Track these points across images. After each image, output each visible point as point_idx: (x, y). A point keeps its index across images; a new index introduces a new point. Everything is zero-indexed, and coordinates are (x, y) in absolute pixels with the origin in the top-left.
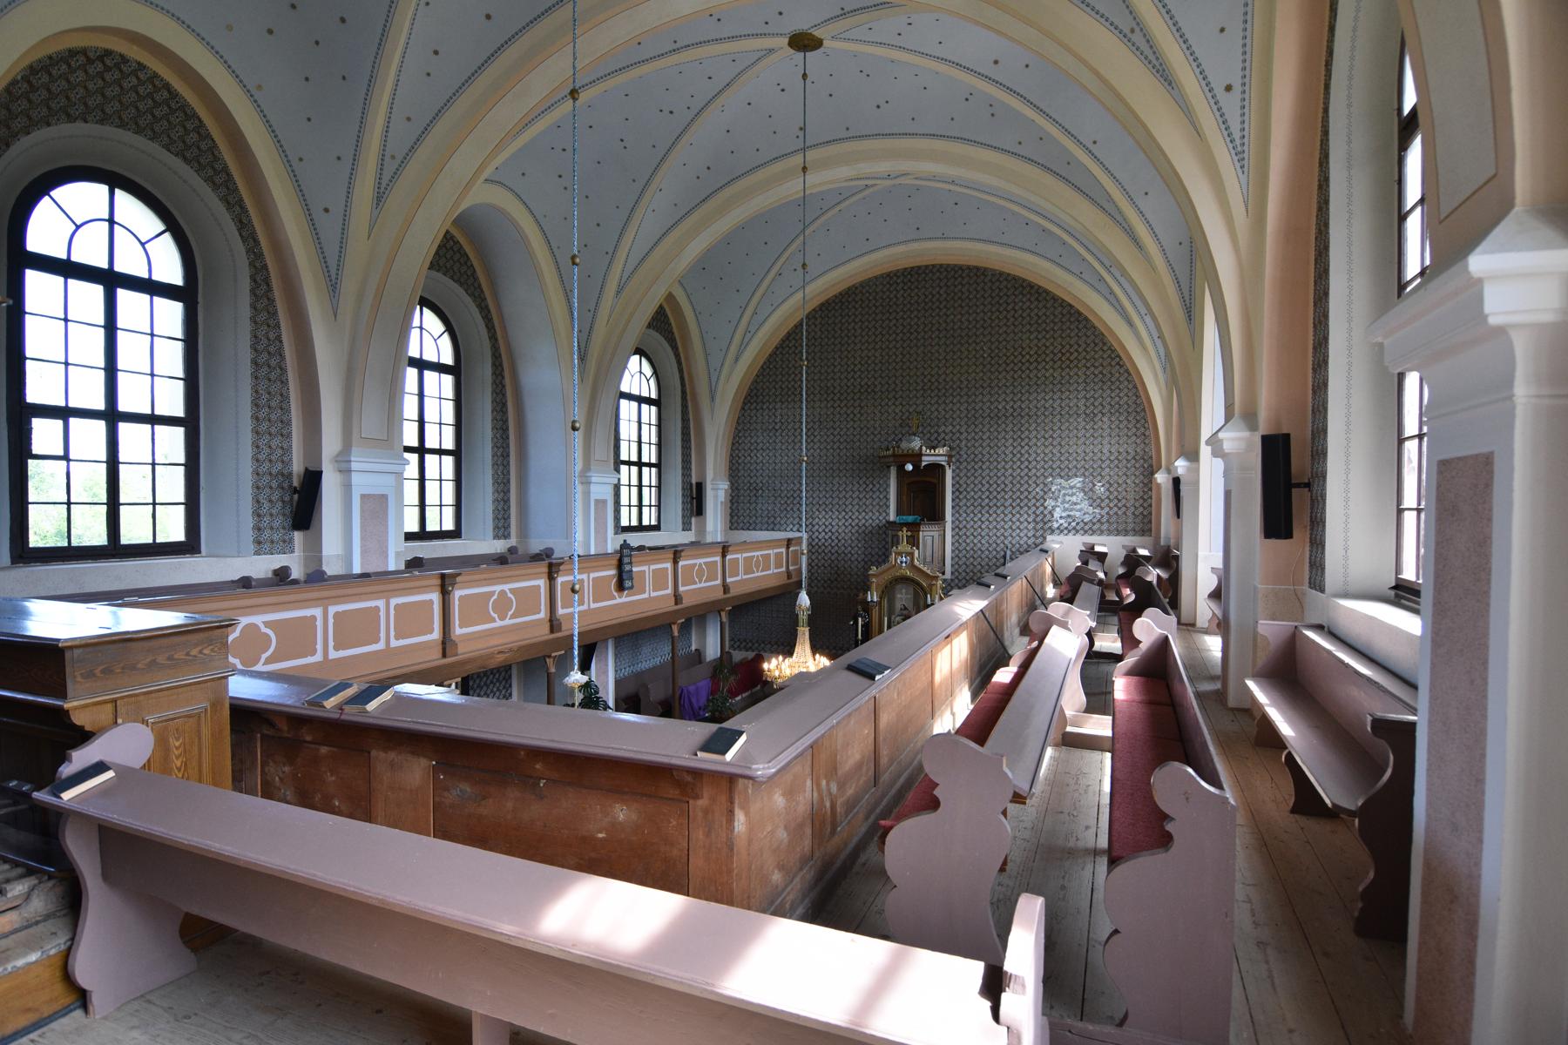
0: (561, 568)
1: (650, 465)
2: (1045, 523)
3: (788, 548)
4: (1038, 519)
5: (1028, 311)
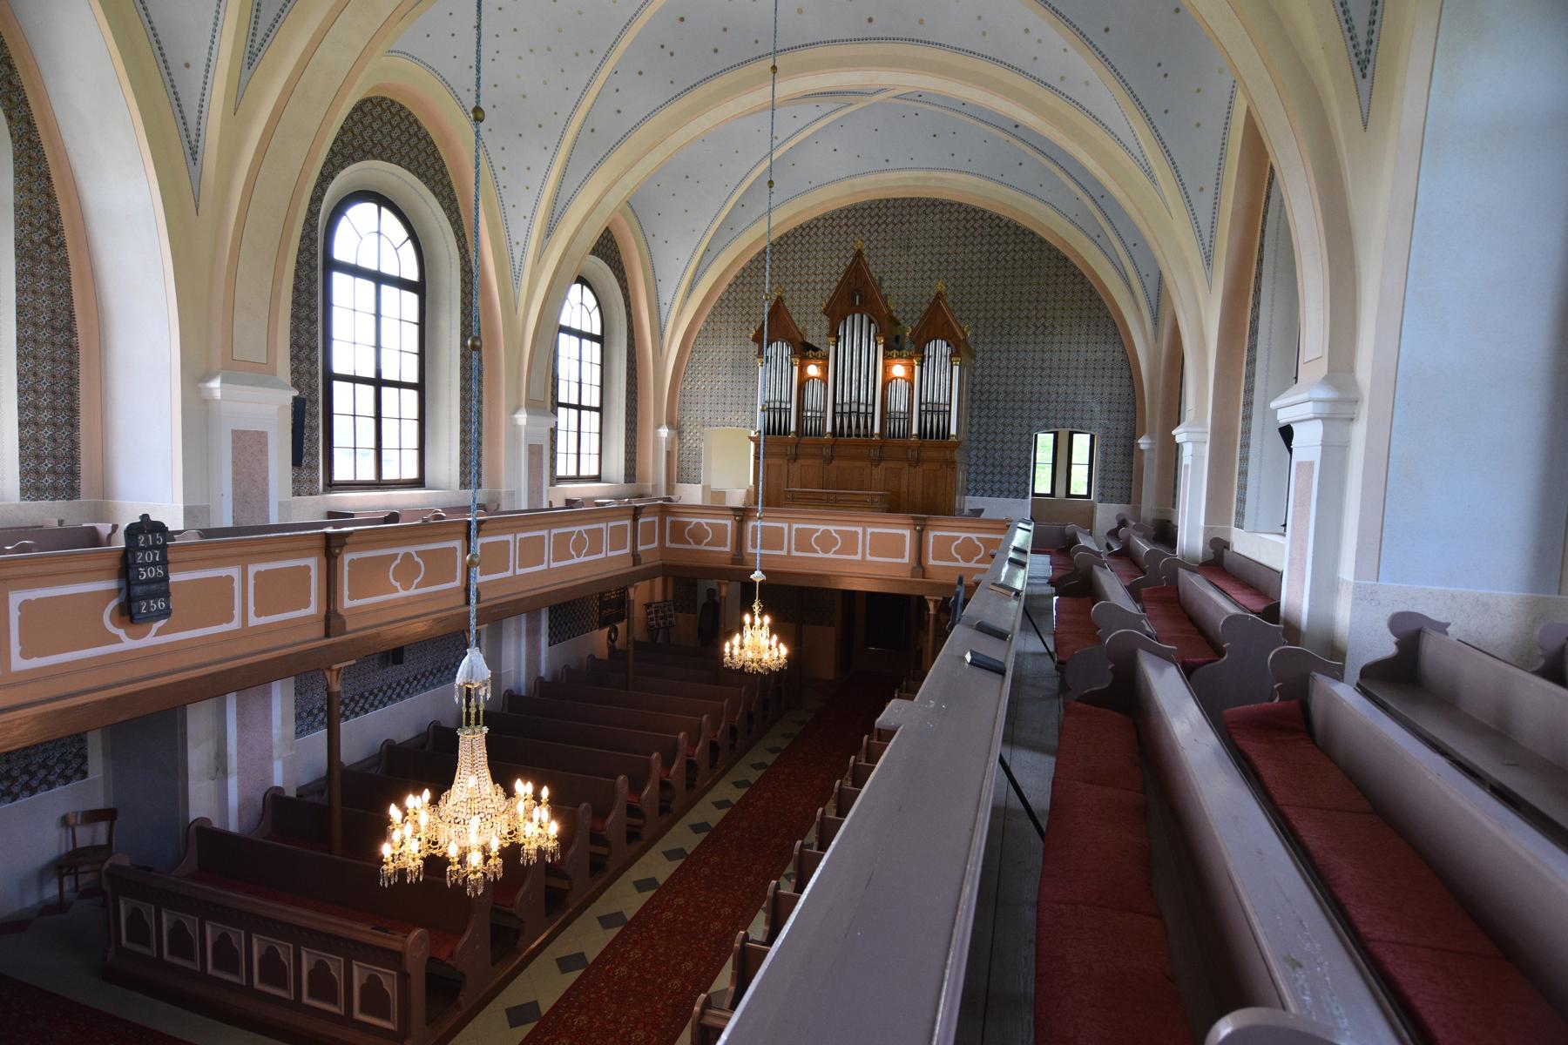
0: (348, 540)
3: (635, 519)
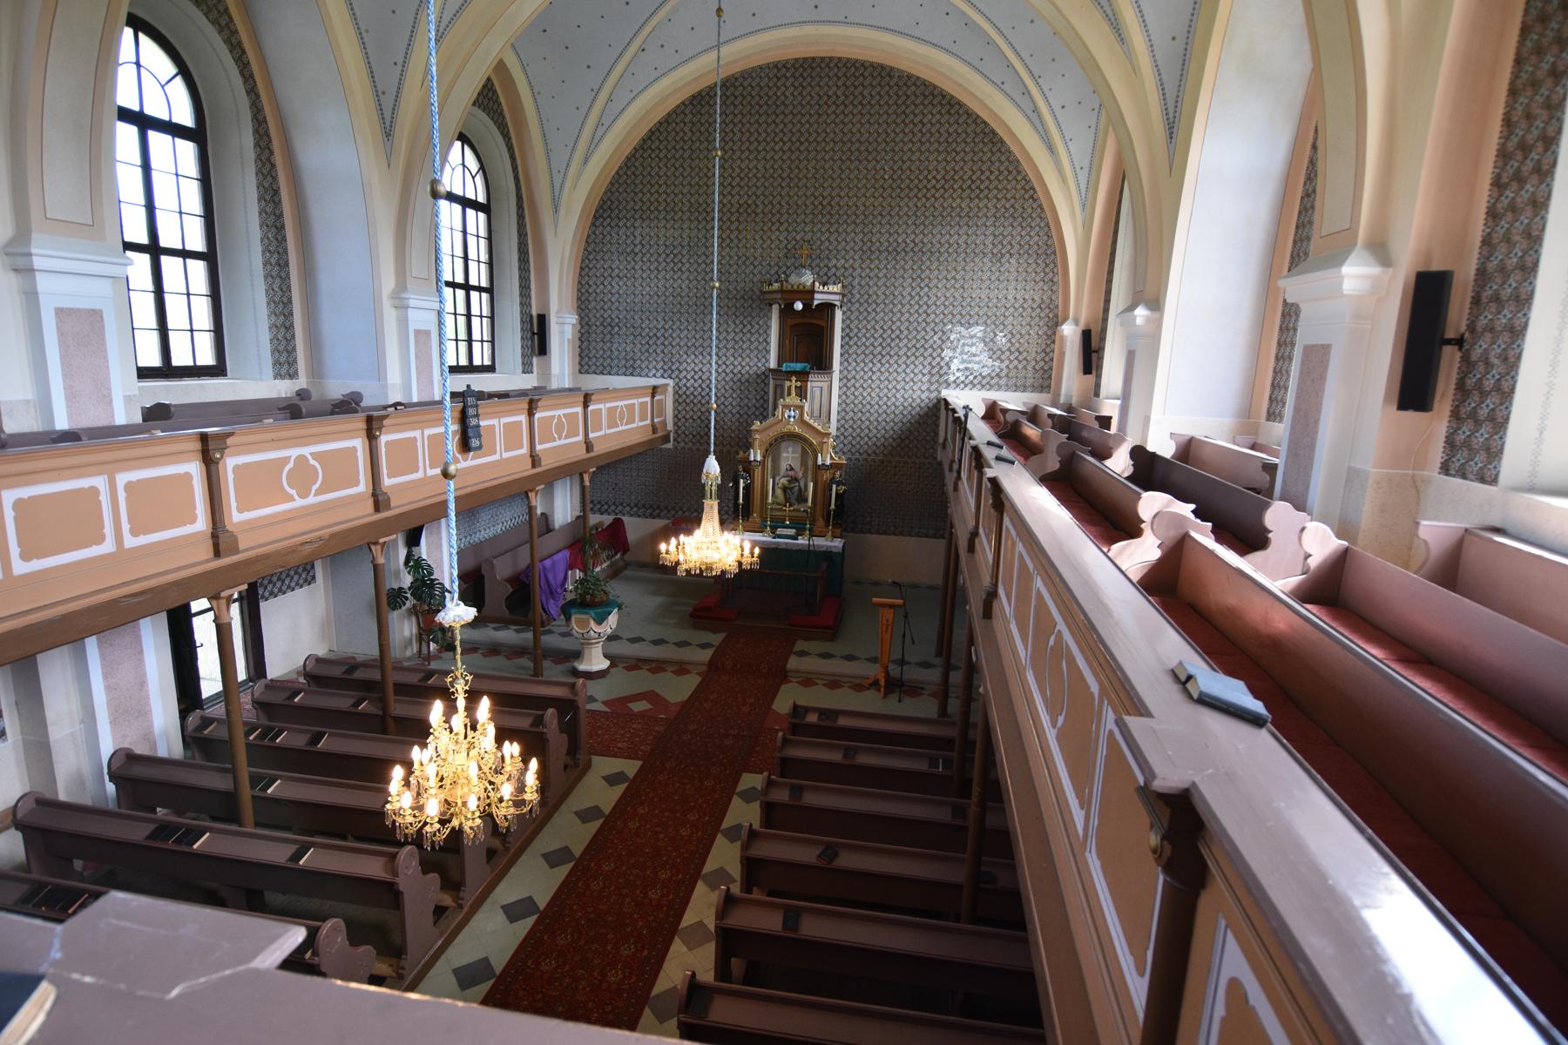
1: (479, 289)
2: (941, 376)
3: (653, 396)
4: (934, 371)
5: (938, 126)
